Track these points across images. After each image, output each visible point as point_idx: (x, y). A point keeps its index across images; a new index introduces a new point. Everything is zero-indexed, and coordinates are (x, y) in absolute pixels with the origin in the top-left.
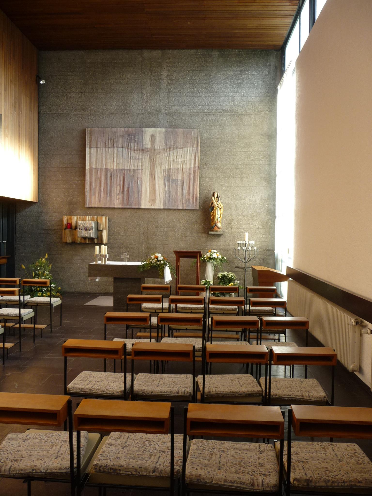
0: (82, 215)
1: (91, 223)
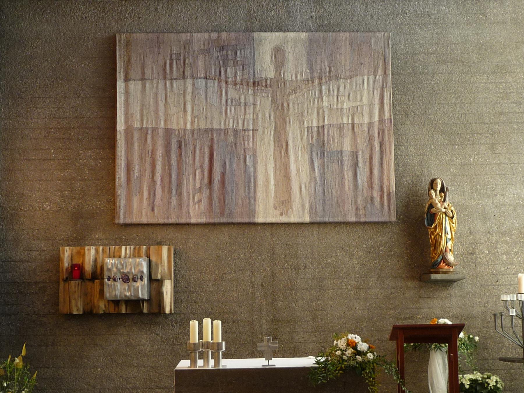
1: (140, 264)
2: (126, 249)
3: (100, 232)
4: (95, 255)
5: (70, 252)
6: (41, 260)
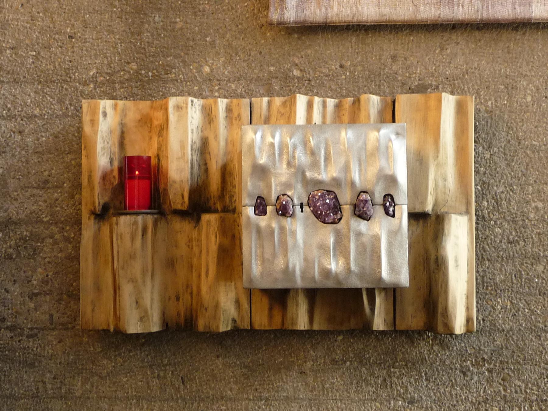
0: (250, 94)
1: (383, 151)
2: (310, 105)
3: (218, 54)
4: (203, 129)
5: (117, 119)
6: (24, 147)
